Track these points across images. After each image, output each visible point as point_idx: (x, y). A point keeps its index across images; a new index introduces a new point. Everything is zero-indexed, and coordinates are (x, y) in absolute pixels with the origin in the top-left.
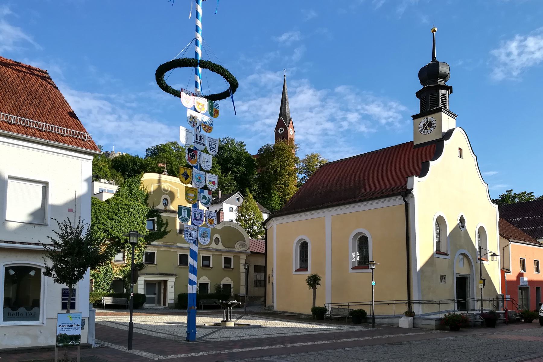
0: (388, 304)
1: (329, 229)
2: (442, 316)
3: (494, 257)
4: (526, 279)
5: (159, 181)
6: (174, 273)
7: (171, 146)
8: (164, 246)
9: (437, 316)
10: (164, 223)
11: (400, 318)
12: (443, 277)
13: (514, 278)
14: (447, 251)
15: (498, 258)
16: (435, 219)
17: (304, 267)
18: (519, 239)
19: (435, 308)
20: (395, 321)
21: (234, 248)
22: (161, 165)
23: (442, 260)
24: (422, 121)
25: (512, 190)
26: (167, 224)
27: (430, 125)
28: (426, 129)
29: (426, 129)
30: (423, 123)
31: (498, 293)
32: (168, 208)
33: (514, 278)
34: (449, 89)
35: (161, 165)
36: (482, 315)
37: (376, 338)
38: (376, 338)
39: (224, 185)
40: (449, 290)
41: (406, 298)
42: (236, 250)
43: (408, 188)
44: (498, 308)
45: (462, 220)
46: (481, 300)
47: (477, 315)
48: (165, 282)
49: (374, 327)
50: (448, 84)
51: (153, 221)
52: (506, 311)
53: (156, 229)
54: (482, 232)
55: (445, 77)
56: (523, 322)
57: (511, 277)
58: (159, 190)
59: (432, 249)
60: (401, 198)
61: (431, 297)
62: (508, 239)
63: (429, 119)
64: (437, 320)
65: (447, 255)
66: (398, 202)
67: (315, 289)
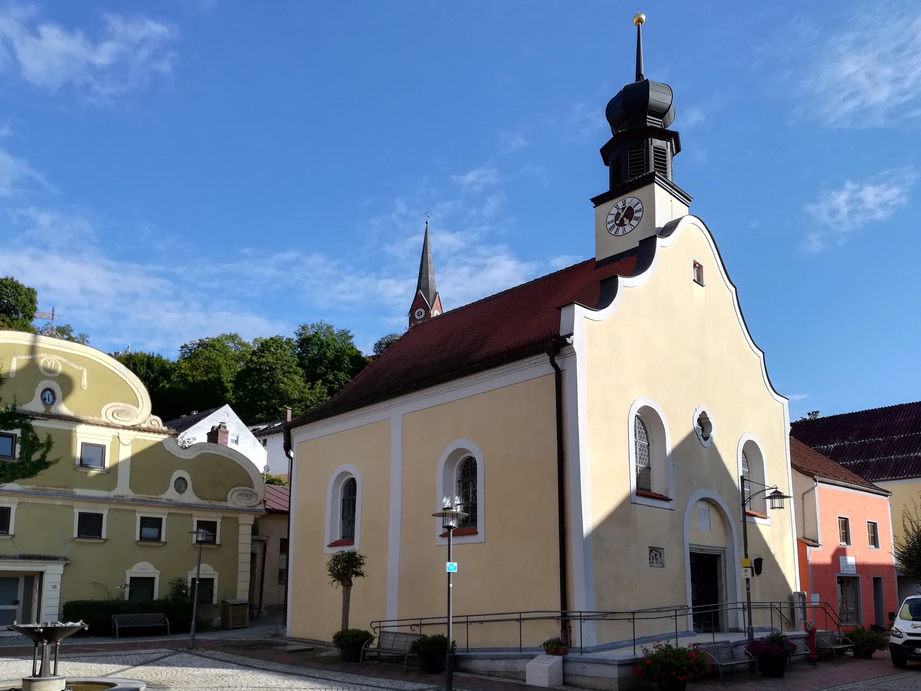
0: (481, 622)
2: (640, 654)
3: (777, 502)
4: (851, 560)
5: (33, 350)
6: (62, 554)
7: (226, 342)
8: (36, 494)
9: (626, 654)
10: (41, 442)
11: (532, 657)
12: (655, 553)
13: (827, 559)
14: (667, 491)
15: (789, 504)
16: (634, 412)
18: (831, 477)
19: (620, 631)
21: (226, 500)
23: (647, 508)
24: (612, 208)
25: (817, 412)
26: (49, 444)
27: (630, 213)
28: (622, 224)
29: (622, 224)
30: (615, 211)
31: (793, 590)
32: (53, 410)
33: (827, 559)
34: (673, 136)
36: (753, 646)
39: (308, 403)
40: (677, 584)
41: (555, 604)
42: (230, 504)
43: (562, 333)
44: (792, 623)
45: (704, 422)
46: (748, 607)
47: (737, 644)
51: (12, 437)
52: (812, 633)
53: (17, 456)
54: (751, 452)
55: (662, 113)
56: (851, 657)
57: (820, 556)
58: (32, 370)
59: (627, 484)
60: (545, 357)
61: (624, 602)
63: (628, 200)
64: (622, 664)
65: (667, 500)
67: (347, 585)
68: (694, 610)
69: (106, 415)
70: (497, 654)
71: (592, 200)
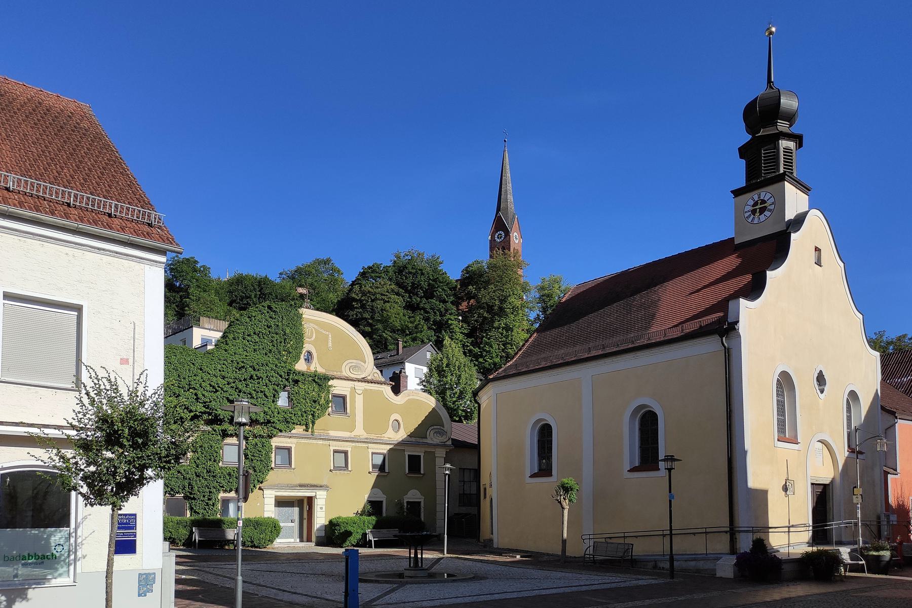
0: (694, 534)
1: (588, 400)
11: (718, 559)
16: (776, 377)
17: (544, 470)
20: (708, 565)
22: (301, 290)
35: (301, 290)
37: (683, 598)
38: (683, 598)
41: (727, 523)
42: (429, 441)
48: (310, 500)
49: (672, 577)
50: (795, 130)
62: (893, 413)
63: (762, 195)
66: (710, 346)
68: (813, 527)
69: (346, 373)
70: (695, 558)
71: (732, 192)
